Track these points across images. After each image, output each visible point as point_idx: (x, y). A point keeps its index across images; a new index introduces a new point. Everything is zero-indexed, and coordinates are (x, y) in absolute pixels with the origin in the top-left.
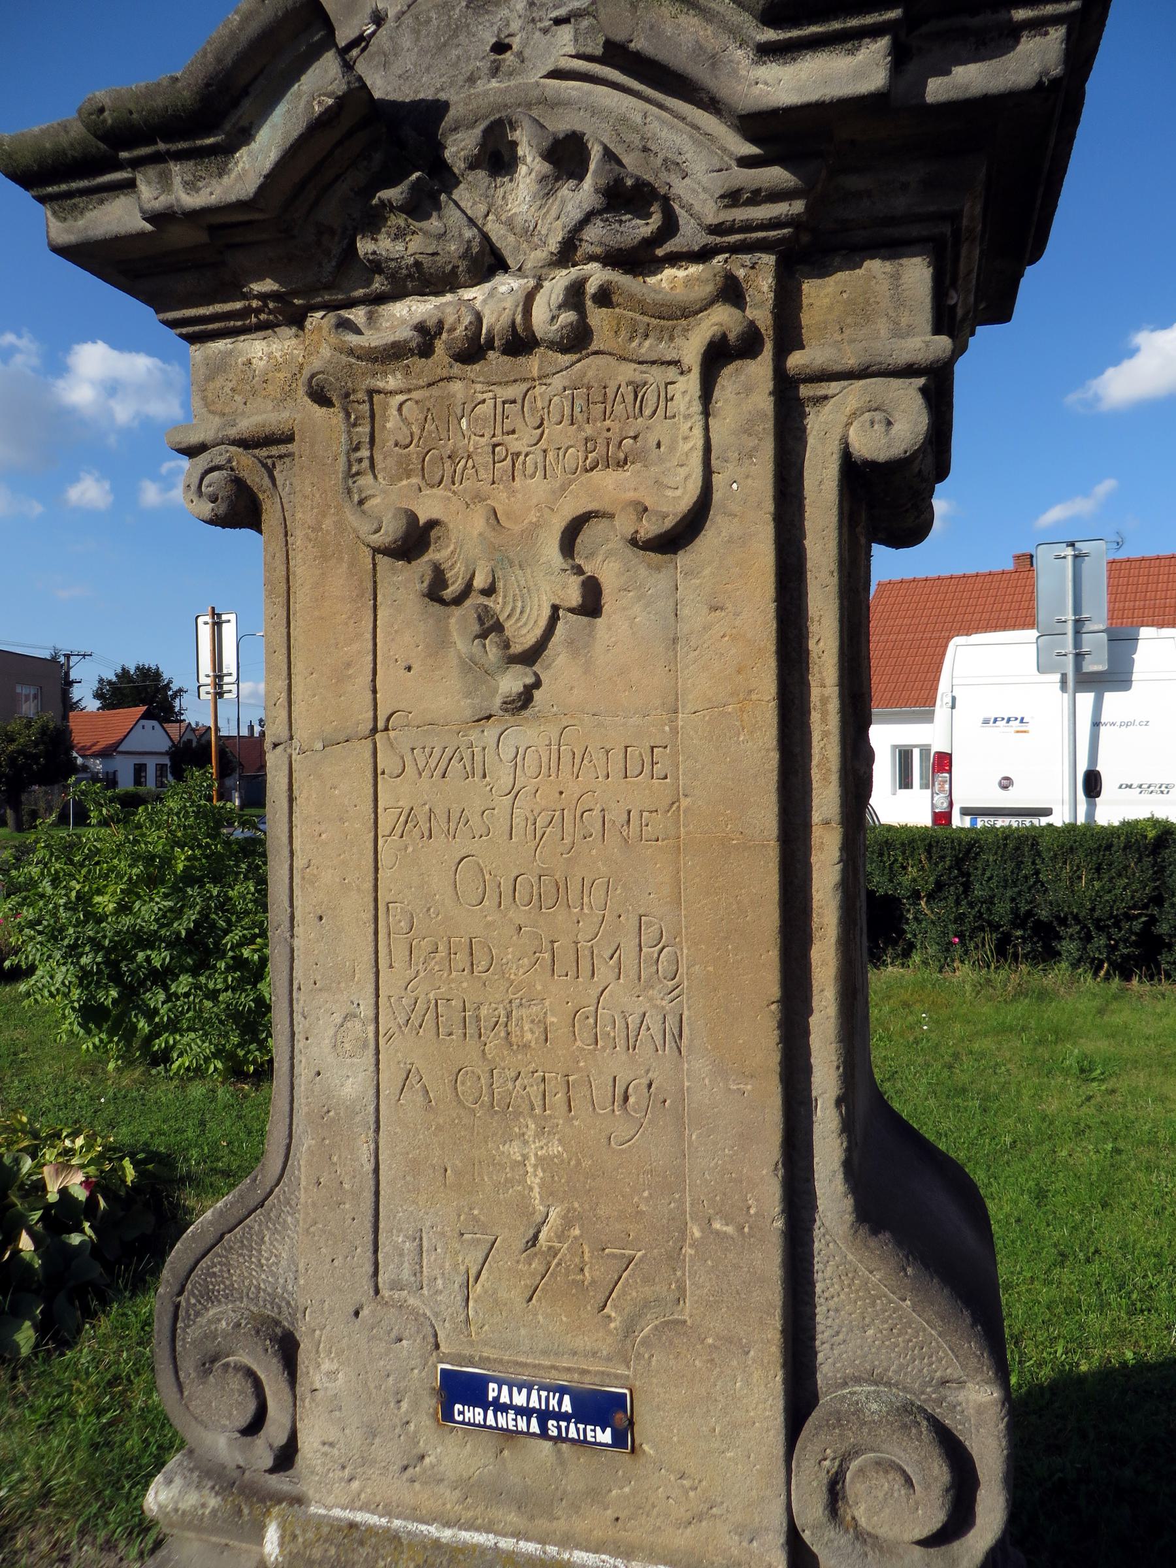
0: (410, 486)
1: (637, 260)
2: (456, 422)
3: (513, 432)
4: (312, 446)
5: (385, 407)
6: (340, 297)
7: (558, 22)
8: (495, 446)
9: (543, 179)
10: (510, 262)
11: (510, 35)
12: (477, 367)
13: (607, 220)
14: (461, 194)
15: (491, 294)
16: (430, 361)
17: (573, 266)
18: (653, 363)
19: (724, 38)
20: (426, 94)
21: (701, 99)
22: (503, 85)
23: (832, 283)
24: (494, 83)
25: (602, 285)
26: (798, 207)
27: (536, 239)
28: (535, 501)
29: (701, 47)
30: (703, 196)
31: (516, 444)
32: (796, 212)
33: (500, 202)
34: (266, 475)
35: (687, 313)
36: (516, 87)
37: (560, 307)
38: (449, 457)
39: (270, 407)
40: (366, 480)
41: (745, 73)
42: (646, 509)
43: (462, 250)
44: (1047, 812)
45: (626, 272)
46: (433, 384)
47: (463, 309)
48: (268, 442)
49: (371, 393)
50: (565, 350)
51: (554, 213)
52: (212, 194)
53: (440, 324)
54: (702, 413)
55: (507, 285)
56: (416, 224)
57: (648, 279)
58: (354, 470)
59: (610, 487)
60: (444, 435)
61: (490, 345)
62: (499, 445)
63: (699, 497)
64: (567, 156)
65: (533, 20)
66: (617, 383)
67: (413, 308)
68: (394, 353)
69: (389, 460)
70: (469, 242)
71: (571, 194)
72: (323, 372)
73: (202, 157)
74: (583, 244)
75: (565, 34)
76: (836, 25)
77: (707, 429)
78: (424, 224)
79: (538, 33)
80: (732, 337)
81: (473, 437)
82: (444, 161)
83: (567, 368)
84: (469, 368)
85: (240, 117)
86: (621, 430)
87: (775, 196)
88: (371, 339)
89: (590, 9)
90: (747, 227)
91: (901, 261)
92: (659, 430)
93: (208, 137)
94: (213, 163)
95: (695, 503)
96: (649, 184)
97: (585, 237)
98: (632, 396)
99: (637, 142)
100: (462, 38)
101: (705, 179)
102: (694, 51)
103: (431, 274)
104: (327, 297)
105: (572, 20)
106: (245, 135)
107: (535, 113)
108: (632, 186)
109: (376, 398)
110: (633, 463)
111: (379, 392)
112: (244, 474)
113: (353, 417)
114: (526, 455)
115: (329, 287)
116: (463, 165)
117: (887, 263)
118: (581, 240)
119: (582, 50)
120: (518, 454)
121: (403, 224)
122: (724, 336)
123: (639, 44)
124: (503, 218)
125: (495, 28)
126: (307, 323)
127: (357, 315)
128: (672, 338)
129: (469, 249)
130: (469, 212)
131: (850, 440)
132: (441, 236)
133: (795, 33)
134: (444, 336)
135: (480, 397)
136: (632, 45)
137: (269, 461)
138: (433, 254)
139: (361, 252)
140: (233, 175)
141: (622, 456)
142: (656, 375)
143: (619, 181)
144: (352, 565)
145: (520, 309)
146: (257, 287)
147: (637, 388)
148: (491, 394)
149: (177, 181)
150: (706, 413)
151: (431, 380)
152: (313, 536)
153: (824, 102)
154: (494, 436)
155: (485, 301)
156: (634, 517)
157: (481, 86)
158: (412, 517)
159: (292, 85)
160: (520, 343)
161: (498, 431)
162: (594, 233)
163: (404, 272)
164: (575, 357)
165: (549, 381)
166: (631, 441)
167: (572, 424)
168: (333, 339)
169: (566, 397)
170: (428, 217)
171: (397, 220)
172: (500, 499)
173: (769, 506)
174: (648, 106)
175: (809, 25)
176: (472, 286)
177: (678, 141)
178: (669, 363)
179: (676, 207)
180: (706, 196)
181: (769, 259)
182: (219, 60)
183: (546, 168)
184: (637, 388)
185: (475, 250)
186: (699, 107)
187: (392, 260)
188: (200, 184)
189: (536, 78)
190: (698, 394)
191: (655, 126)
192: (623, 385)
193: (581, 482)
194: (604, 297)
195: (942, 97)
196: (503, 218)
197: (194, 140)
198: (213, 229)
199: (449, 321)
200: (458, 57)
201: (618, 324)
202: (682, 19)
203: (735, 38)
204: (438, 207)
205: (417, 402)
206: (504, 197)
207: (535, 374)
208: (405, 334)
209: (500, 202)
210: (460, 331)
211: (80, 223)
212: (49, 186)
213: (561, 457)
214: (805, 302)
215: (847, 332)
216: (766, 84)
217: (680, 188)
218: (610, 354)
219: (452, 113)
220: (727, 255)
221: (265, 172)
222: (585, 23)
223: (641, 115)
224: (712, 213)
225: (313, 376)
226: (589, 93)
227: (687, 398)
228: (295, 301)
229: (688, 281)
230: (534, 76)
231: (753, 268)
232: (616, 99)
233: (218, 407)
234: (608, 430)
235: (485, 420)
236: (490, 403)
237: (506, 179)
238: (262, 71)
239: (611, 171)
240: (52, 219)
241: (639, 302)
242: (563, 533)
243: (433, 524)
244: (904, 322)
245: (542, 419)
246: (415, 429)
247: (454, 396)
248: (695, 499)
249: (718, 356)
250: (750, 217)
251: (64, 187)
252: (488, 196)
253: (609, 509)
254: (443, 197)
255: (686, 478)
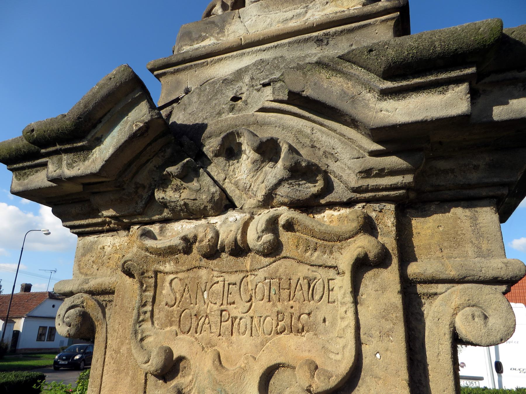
0: (171, 331)
1: (309, 206)
2: (201, 293)
3: (234, 303)
4: (123, 300)
5: (163, 282)
6: (146, 219)
7: (264, 85)
8: (222, 311)
9: (254, 162)
10: (237, 204)
11: (241, 94)
12: (215, 262)
13: (291, 184)
14: (212, 169)
15: (224, 222)
16: (190, 256)
17: (272, 208)
18: (320, 266)
19: (359, 88)
20: (199, 121)
21: (346, 120)
22: (235, 116)
23: (431, 221)
24: (231, 115)
25: (287, 220)
26: (409, 178)
27: (250, 193)
28: (244, 351)
29: (345, 93)
30: (348, 171)
31: (235, 311)
32: (407, 181)
33: (231, 173)
34: (100, 311)
35: (341, 238)
36: (242, 116)
37: (263, 231)
38: (195, 315)
39: (109, 273)
40: (147, 325)
41: (373, 105)
42: (316, 368)
43: (209, 198)
44: (481, 379)
45: (302, 212)
46: (191, 269)
47: (208, 229)
48: (103, 294)
49: (156, 272)
50: (266, 255)
51: (260, 179)
52: (79, 169)
53: (195, 237)
54: (353, 303)
55: (234, 217)
56: (186, 184)
57: (316, 216)
58: (141, 319)
59: (293, 347)
60: (193, 301)
61: (223, 250)
62: (225, 310)
63: (353, 363)
64: (268, 150)
65: (253, 86)
66: (297, 277)
67: (184, 226)
68: (170, 252)
69: (162, 313)
70: (213, 194)
71: (271, 169)
72: (131, 260)
73: (77, 152)
74: (277, 196)
75: (268, 90)
76: (432, 78)
77: (356, 313)
78: (190, 185)
79: (255, 92)
80: (371, 256)
81: (210, 304)
82: (203, 153)
83: (267, 266)
84: (211, 262)
85: (96, 133)
86: (300, 308)
87: (393, 172)
88: (161, 243)
89: (281, 78)
90: (377, 189)
91: (476, 209)
92: (324, 310)
93: (80, 142)
94: (82, 154)
95: (351, 368)
96: (316, 165)
97: (278, 193)
98: (307, 286)
99: (308, 143)
100: (219, 96)
101: (350, 163)
102: (341, 95)
103: (193, 210)
104: (140, 219)
105: (272, 84)
106: (98, 141)
107: (251, 129)
108: (306, 166)
109: (159, 275)
110: (308, 331)
111: (161, 272)
112: (89, 310)
113: (145, 286)
114: (241, 319)
115: (141, 214)
116: (211, 155)
117: (467, 210)
118: (276, 194)
119: (277, 98)
120: (236, 318)
121: (179, 184)
122: (366, 255)
123: (308, 92)
124: (233, 181)
125: (235, 91)
126: (131, 229)
127: (155, 228)
128: (331, 252)
129: (213, 197)
130: (215, 178)
131: (456, 325)
132: (198, 191)
133: (404, 83)
134: (197, 243)
135: (216, 279)
136: (304, 93)
137: (104, 303)
138: (194, 200)
139: (157, 198)
140: (90, 161)
141: (300, 326)
142: (321, 274)
143: (297, 164)
144: (133, 378)
145: (240, 231)
146: (105, 213)
147: (309, 281)
148: (222, 279)
149: (64, 163)
150: (356, 302)
151: (189, 267)
152: (114, 355)
153: (426, 121)
154: (222, 304)
155: (221, 225)
156: (308, 374)
157: (224, 116)
158: (169, 352)
159: (124, 118)
160: (240, 250)
161: (225, 302)
162: (284, 191)
163: (179, 208)
164: (272, 260)
165: (256, 273)
166: (306, 316)
167: (269, 301)
168: (138, 243)
169: (266, 284)
170: (191, 180)
171: (177, 182)
172: (223, 347)
173: (404, 375)
174: (314, 125)
175: (414, 78)
176: (216, 216)
177: (332, 142)
178: (330, 267)
179: (332, 177)
180: (350, 172)
181: (391, 207)
182: (85, 107)
183: (256, 156)
184: (309, 281)
185: (217, 198)
186: (344, 125)
187: (173, 202)
188: (74, 165)
189: (253, 112)
190: (350, 290)
191: (318, 135)
192: (301, 279)
193: (274, 342)
194: (289, 226)
195: (505, 117)
196: (233, 181)
197: (73, 144)
198: (84, 185)
199: (200, 236)
200: (216, 104)
201: (298, 242)
202: (333, 79)
203: (366, 87)
204: (198, 175)
205: (180, 280)
206: (233, 171)
207: (248, 268)
208: (176, 241)
209: (231, 173)
210: (205, 242)
211: (26, 181)
212: (15, 164)
213: (262, 323)
214: (414, 231)
215: (445, 251)
216: (387, 111)
217: (333, 167)
218: (293, 259)
219: (208, 129)
220: (364, 204)
221: (105, 159)
222: (278, 85)
223: (310, 129)
224: (354, 181)
225: (125, 262)
226: (281, 119)
227: (343, 291)
228: (124, 220)
229: (340, 218)
230: (251, 111)
231: (381, 211)
232: (296, 122)
233: (84, 271)
234: (292, 307)
235: (218, 294)
236: (221, 284)
237: (235, 161)
238: (109, 111)
239: (293, 158)
240: (15, 179)
241: (311, 230)
242: (261, 378)
243: (181, 359)
244: (484, 247)
245: (251, 296)
246: (178, 296)
247: (201, 278)
248: (351, 365)
249: (361, 266)
250: (378, 183)
251: (21, 165)
252: (224, 170)
253: (291, 363)
254: (201, 170)
255: (344, 347)
